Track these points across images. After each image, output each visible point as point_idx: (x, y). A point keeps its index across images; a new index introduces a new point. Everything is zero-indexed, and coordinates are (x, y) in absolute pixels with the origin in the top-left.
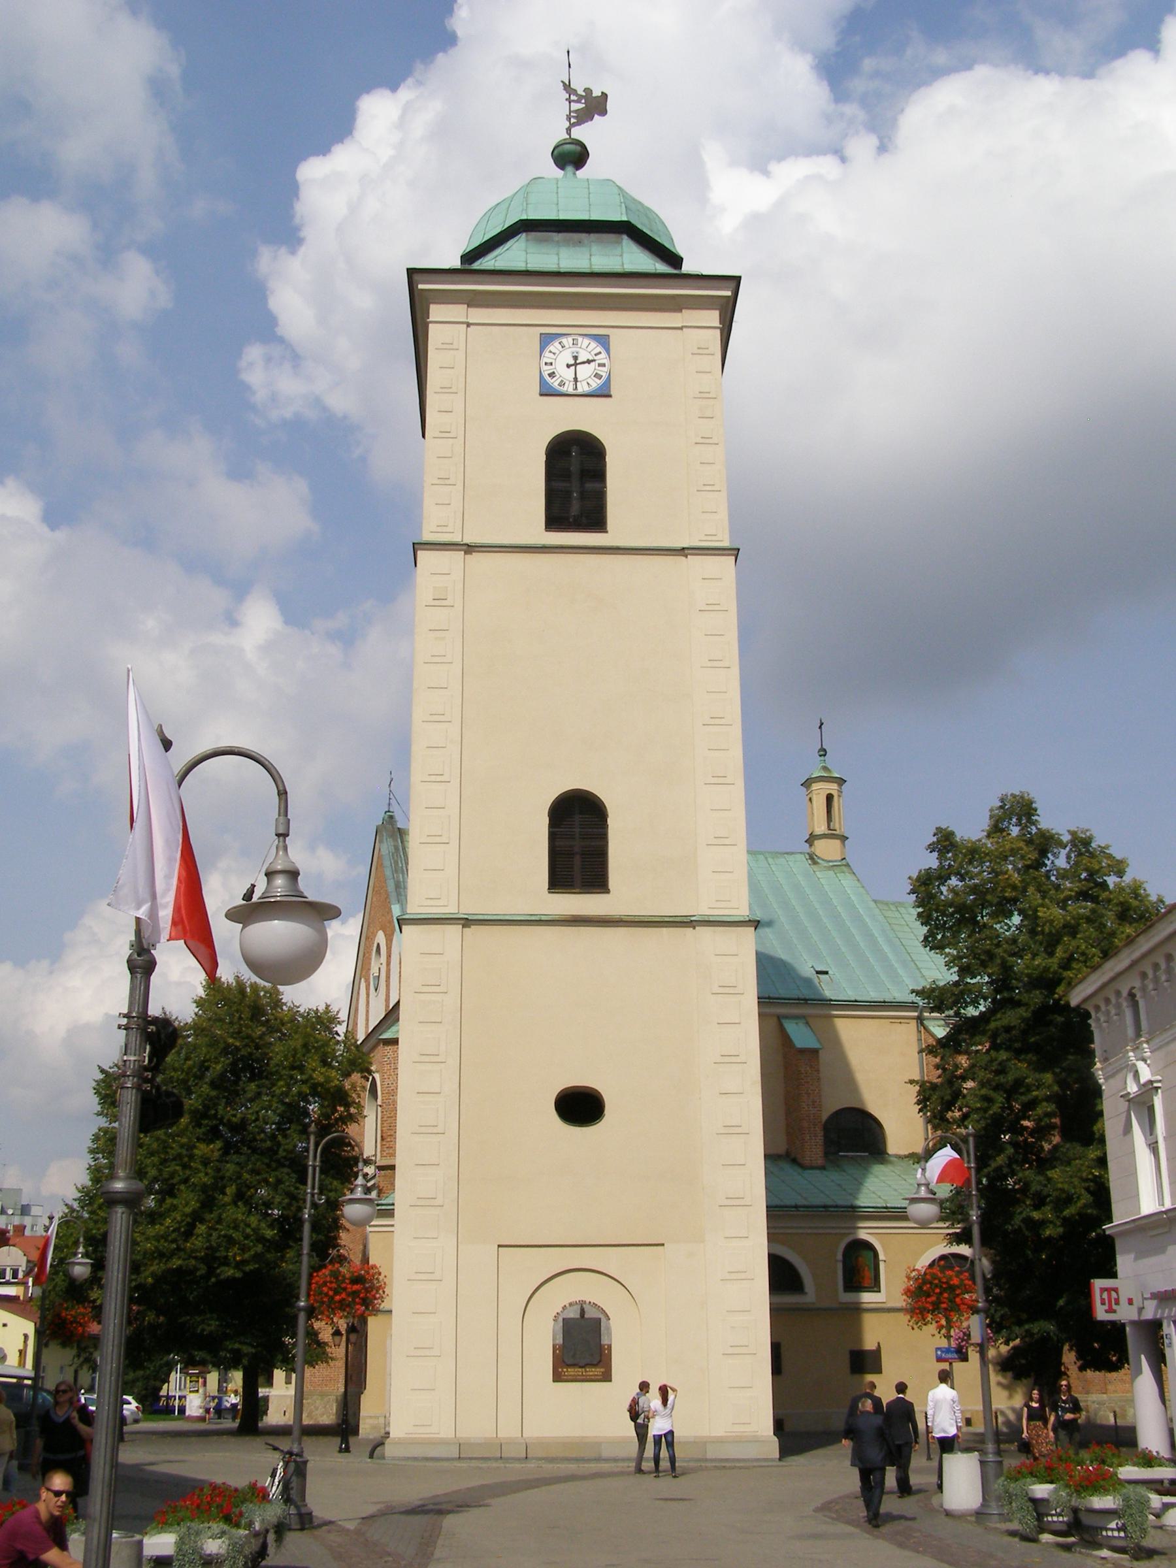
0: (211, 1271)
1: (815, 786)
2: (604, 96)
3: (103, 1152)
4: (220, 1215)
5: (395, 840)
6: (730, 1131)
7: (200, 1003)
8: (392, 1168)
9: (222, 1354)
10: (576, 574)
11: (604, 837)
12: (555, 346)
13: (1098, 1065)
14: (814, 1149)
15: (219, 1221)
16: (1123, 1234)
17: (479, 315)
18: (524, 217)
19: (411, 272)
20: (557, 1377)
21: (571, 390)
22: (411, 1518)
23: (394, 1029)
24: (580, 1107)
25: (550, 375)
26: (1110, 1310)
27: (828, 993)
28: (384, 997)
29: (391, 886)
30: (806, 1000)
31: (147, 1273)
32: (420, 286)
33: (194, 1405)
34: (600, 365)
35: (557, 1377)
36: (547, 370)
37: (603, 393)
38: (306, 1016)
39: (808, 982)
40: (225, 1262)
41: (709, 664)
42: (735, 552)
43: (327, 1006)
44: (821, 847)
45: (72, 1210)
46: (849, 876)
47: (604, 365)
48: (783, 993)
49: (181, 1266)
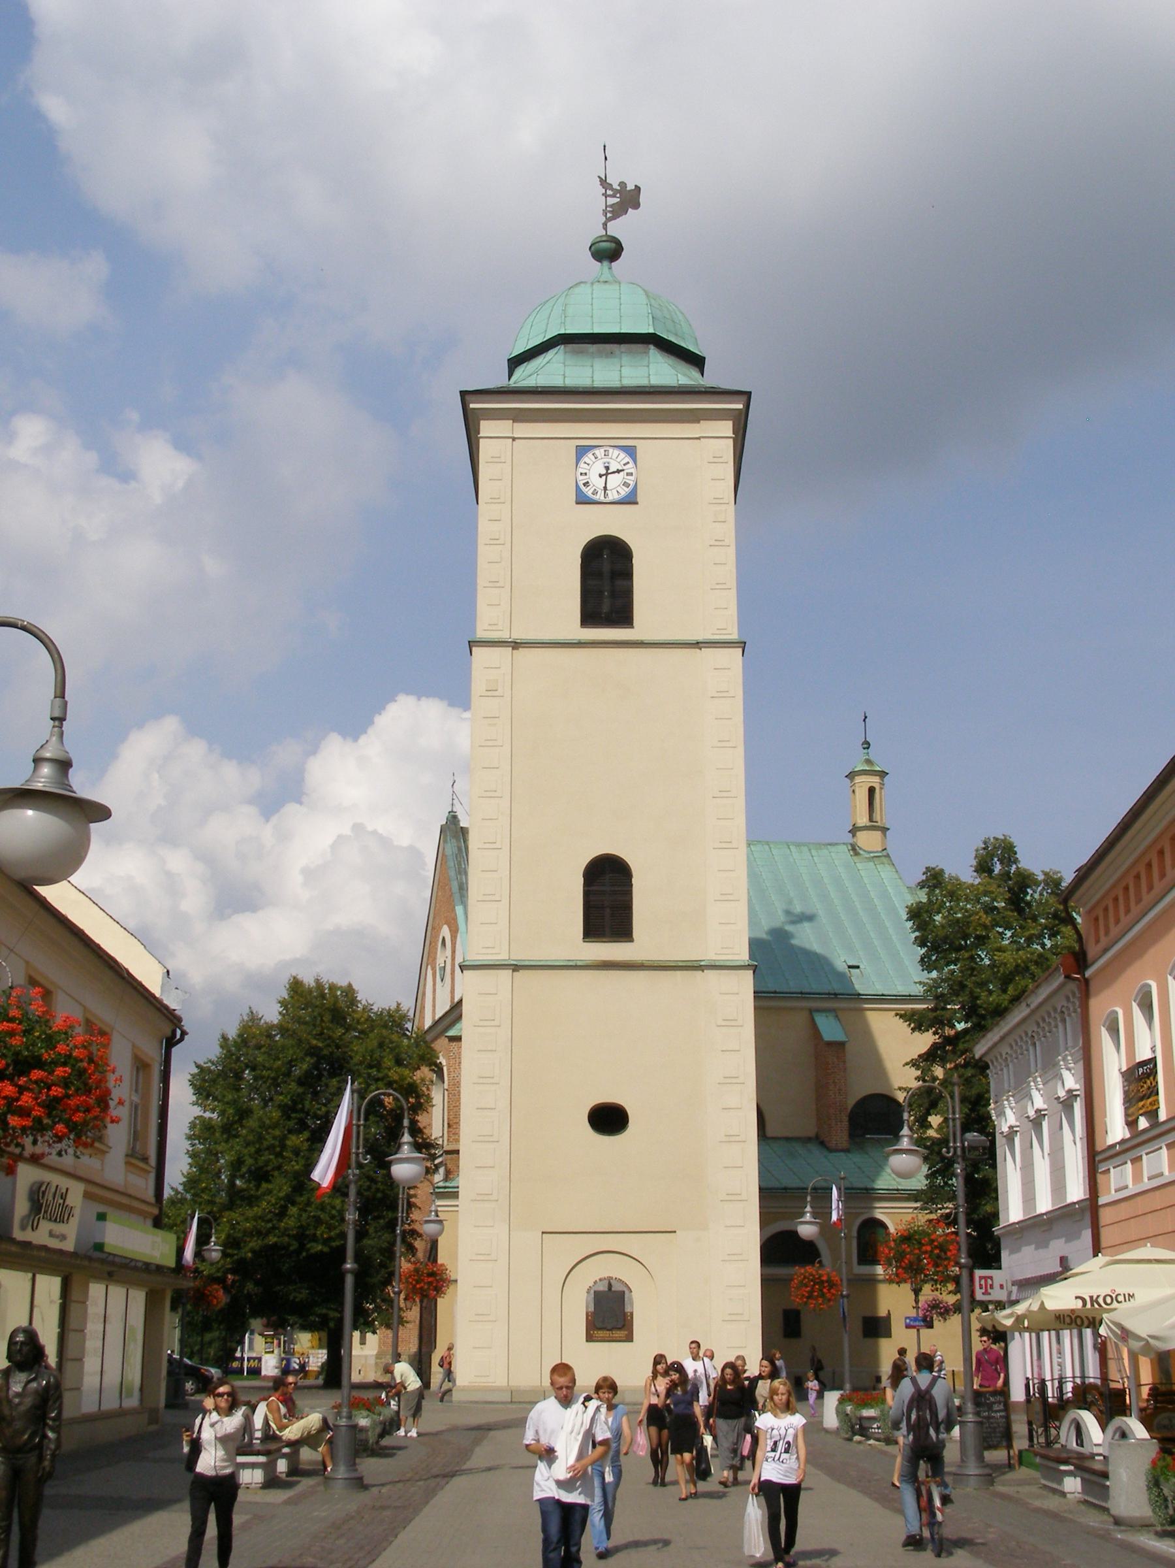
0: (302, 1247)
1: (858, 779)
2: (638, 188)
3: (199, 1138)
4: (309, 1200)
5: (458, 840)
6: (730, 1139)
7: (283, 1003)
8: (457, 1152)
9: (312, 1318)
10: (609, 665)
11: (629, 893)
12: (588, 458)
13: (992, 1106)
14: (840, 1135)
15: (309, 1203)
16: (1004, 1234)
17: (522, 429)
18: (562, 332)
19: (463, 394)
20: (590, 1338)
21: (602, 499)
22: (474, 1432)
23: (458, 1026)
24: (609, 1119)
25: (584, 485)
26: (986, 1293)
27: (860, 988)
28: (449, 989)
29: (455, 886)
30: (835, 994)
31: (247, 1249)
32: (472, 406)
33: (270, 1366)
34: (628, 474)
35: (590, 1338)
36: (582, 480)
37: (630, 500)
38: (380, 1015)
39: (841, 976)
40: (314, 1238)
41: (719, 744)
42: (743, 645)
43: (399, 1004)
44: (863, 839)
45: (177, 1192)
46: (888, 868)
47: (631, 474)
48: (815, 988)
49: (276, 1243)
